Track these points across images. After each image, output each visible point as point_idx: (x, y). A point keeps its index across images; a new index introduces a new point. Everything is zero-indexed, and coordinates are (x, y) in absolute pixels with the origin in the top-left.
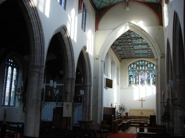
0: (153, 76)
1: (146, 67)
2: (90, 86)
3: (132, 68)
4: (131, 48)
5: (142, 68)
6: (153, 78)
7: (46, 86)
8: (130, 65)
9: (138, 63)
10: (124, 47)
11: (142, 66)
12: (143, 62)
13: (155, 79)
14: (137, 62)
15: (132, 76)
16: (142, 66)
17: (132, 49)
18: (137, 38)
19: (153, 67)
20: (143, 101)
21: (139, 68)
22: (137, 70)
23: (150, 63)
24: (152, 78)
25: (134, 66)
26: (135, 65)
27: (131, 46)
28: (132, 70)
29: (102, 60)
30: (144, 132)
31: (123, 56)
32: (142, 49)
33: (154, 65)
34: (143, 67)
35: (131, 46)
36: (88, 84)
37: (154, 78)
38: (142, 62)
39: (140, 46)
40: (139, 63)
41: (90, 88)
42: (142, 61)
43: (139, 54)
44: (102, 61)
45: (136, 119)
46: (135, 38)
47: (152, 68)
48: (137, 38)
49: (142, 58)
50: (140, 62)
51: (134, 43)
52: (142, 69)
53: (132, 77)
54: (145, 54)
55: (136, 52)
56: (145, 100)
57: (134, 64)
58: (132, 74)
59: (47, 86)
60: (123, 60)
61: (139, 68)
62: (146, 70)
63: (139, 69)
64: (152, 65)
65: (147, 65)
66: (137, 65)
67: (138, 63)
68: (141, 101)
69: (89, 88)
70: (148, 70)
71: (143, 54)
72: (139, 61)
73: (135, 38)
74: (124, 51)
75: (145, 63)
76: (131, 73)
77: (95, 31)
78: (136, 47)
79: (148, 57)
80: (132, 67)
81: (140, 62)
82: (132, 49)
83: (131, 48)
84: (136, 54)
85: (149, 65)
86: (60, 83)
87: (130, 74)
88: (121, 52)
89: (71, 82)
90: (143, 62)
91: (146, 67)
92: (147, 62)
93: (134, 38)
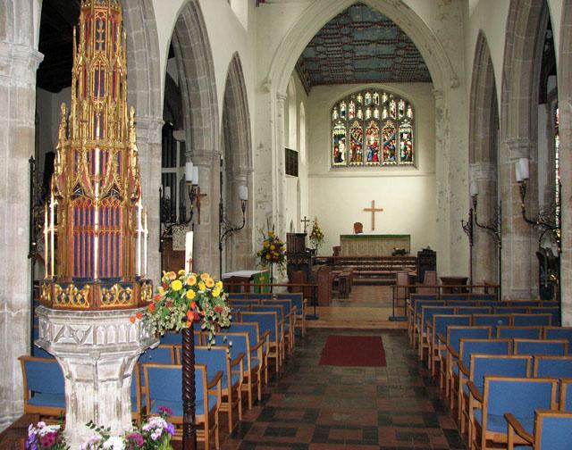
0: (405, 136)
1: (385, 111)
2: (249, 172)
3: (344, 113)
4: (345, 51)
5: (372, 113)
6: (406, 144)
7: (163, 174)
8: (337, 105)
9: (360, 98)
10: (324, 49)
11: (372, 107)
12: (376, 95)
13: (410, 147)
14: (357, 94)
15: (343, 136)
16: (372, 107)
17: (347, 55)
18: (369, 24)
19: (406, 111)
20: (376, 213)
21: (364, 112)
22: (359, 120)
23: (397, 99)
24: (403, 143)
25: (348, 108)
26: (352, 105)
27: (347, 48)
28: (343, 120)
29: (281, 94)
30: (227, 413)
31: (317, 76)
32: (380, 56)
33: (407, 104)
34: (376, 112)
35: (347, 48)
36: (243, 166)
37: (409, 143)
38: (372, 96)
39: (373, 45)
40: (364, 98)
41: (247, 178)
42: (372, 91)
43: (366, 70)
44: (278, 98)
45: (361, 264)
46: (363, 23)
47: (401, 112)
48: (369, 24)
49: (373, 81)
50: (368, 96)
51: (357, 36)
52: (372, 118)
53: (344, 142)
54: (385, 70)
55: (360, 64)
56: (382, 210)
57: (348, 100)
58: (343, 132)
59: (172, 166)
60: (316, 90)
61: (364, 112)
62: (385, 120)
63: (364, 116)
64: (402, 105)
65: (387, 104)
66: (358, 106)
67: (360, 98)
68: (370, 213)
69: (244, 179)
70: (392, 120)
71: (378, 70)
72: (363, 93)
73: (363, 23)
74: (322, 62)
75: (381, 97)
76: (339, 127)
77: (257, 5)
78: (361, 51)
79: (391, 80)
80: (343, 110)
81: (368, 96)
82: (347, 55)
83: (345, 51)
84: (355, 70)
85: (393, 105)
86: (167, 167)
87: (336, 132)
88: (313, 66)
89: (210, 163)
90: (376, 95)
91: (385, 111)
92: (388, 94)
93: (360, 23)
